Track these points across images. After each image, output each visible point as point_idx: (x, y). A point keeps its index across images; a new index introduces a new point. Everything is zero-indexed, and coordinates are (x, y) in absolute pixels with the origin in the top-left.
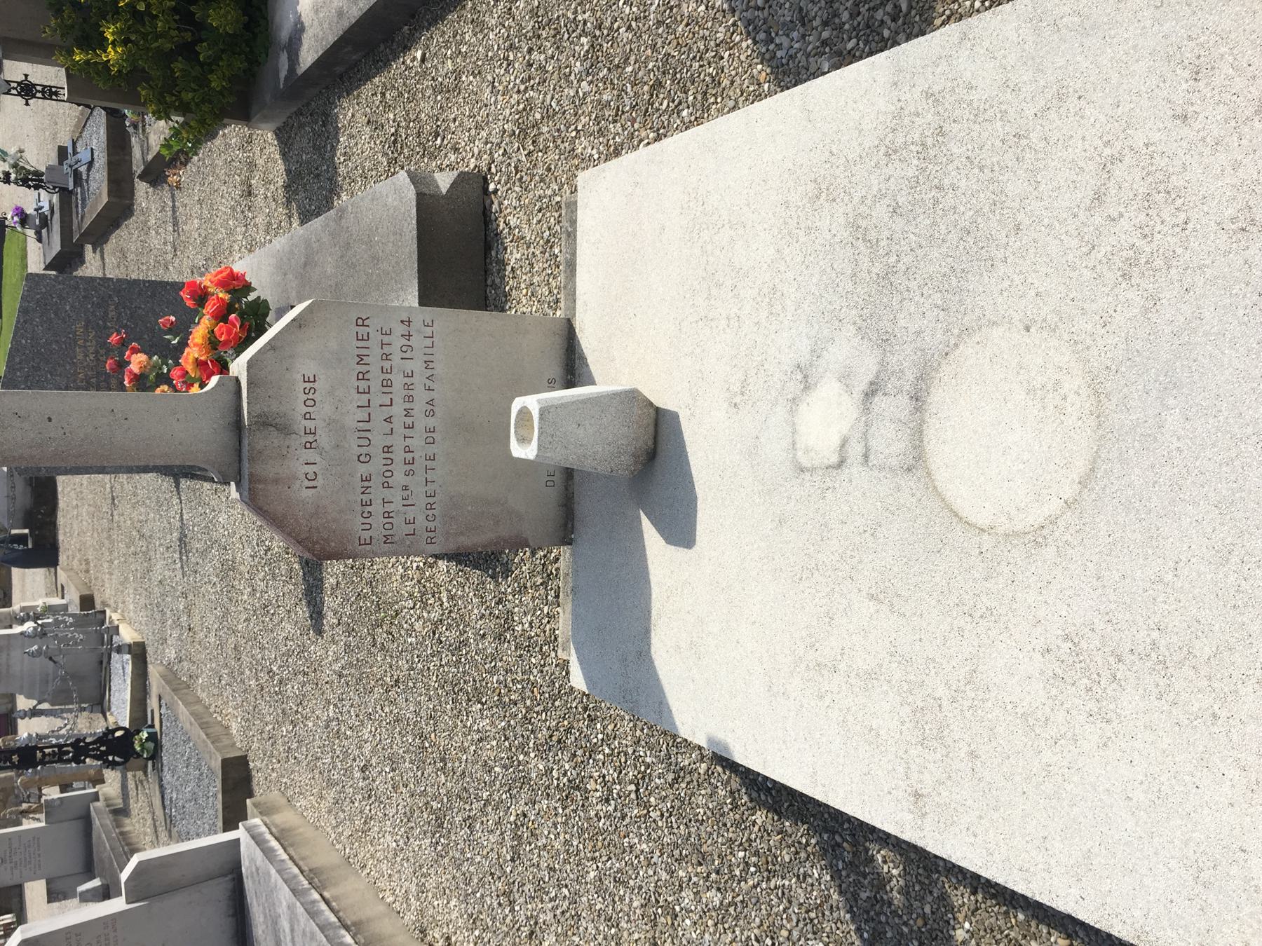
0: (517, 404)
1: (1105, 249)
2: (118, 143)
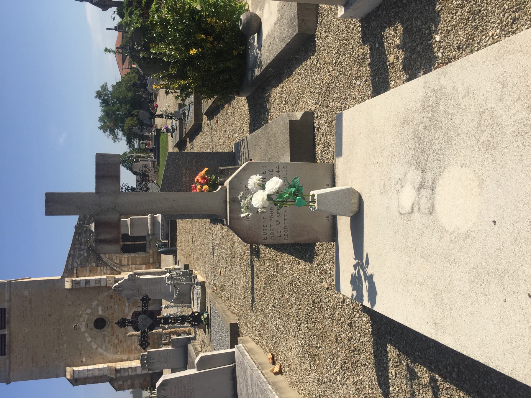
0: (312, 193)
1: (481, 141)
2: (198, 104)
